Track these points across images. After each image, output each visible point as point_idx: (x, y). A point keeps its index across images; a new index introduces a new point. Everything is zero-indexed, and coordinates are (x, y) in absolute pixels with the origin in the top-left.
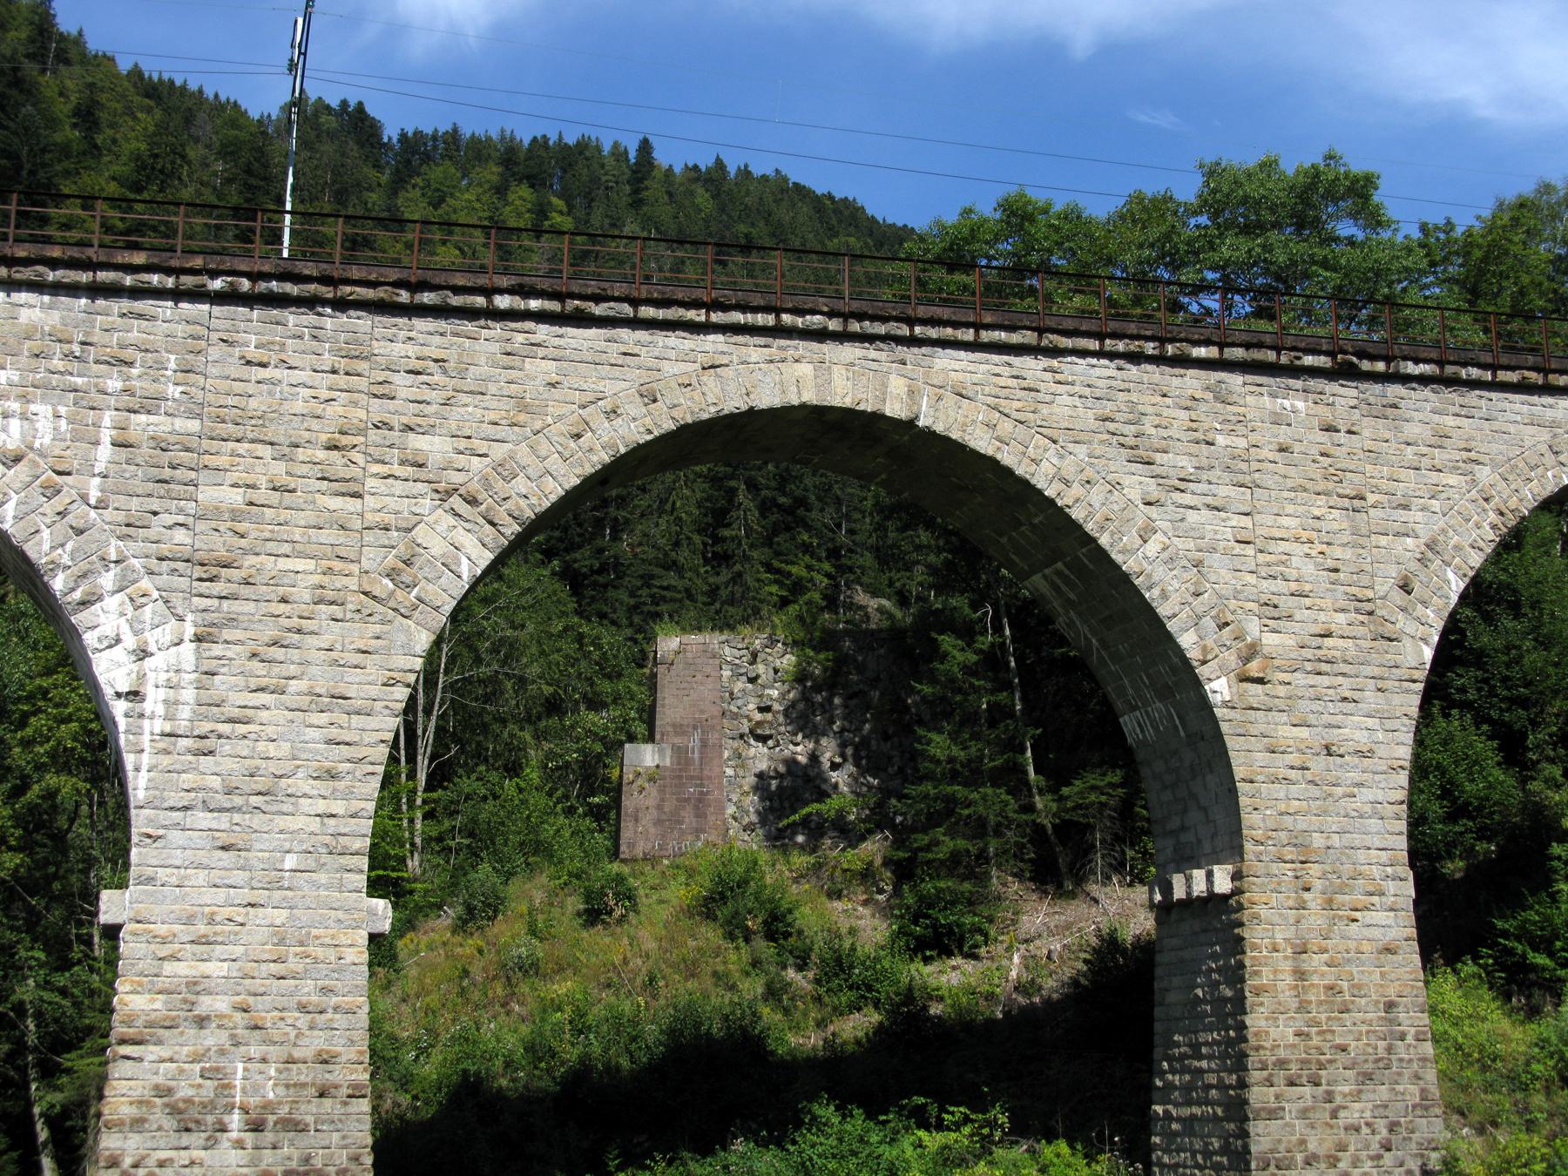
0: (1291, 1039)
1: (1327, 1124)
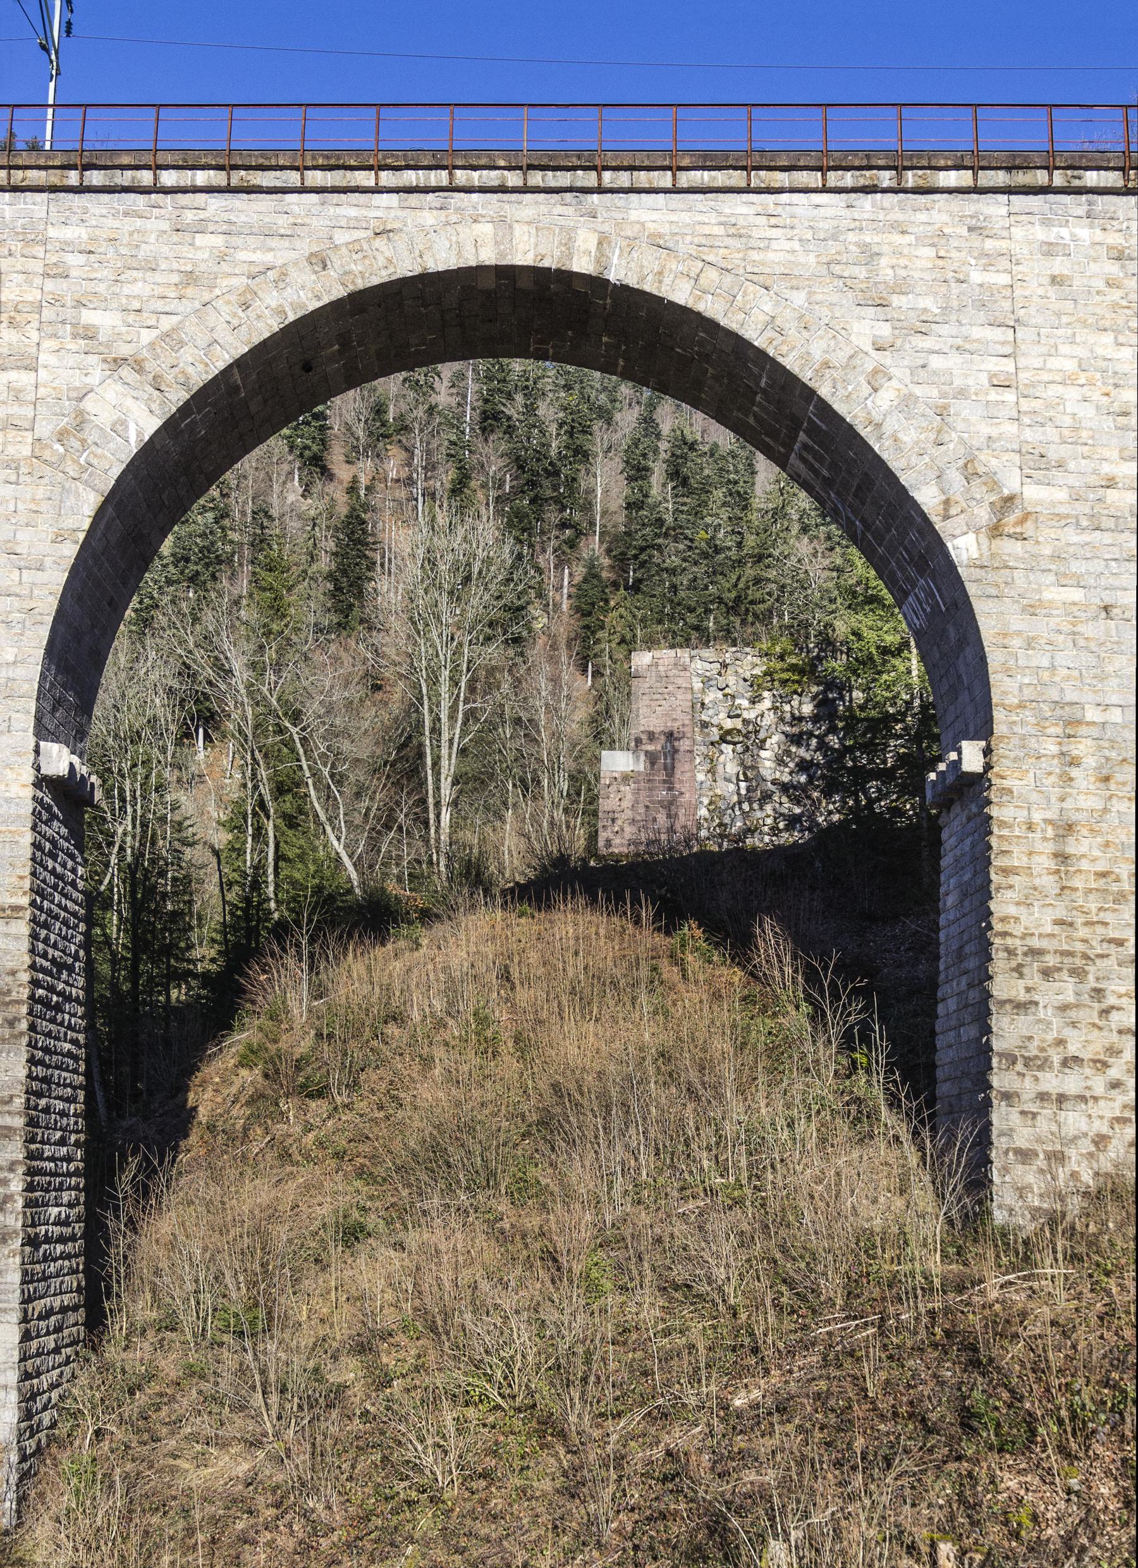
0: (1049, 929)
1: (1094, 1025)
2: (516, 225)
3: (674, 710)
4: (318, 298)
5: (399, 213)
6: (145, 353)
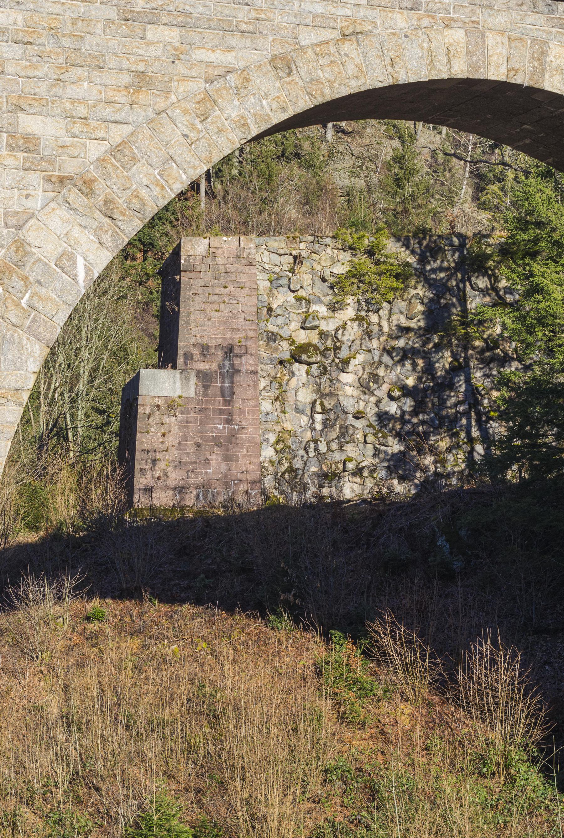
2: (489, 34)
3: (234, 316)
4: (284, 110)
5: (369, 13)
6: (93, 173)
